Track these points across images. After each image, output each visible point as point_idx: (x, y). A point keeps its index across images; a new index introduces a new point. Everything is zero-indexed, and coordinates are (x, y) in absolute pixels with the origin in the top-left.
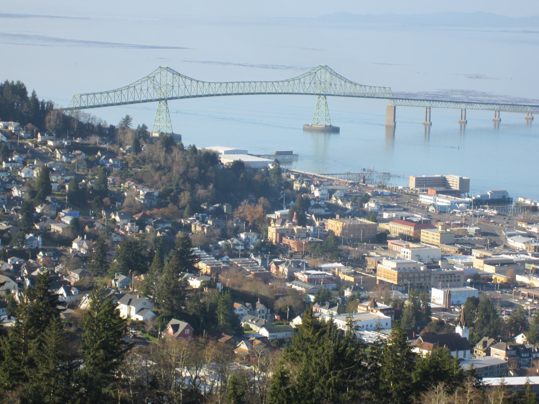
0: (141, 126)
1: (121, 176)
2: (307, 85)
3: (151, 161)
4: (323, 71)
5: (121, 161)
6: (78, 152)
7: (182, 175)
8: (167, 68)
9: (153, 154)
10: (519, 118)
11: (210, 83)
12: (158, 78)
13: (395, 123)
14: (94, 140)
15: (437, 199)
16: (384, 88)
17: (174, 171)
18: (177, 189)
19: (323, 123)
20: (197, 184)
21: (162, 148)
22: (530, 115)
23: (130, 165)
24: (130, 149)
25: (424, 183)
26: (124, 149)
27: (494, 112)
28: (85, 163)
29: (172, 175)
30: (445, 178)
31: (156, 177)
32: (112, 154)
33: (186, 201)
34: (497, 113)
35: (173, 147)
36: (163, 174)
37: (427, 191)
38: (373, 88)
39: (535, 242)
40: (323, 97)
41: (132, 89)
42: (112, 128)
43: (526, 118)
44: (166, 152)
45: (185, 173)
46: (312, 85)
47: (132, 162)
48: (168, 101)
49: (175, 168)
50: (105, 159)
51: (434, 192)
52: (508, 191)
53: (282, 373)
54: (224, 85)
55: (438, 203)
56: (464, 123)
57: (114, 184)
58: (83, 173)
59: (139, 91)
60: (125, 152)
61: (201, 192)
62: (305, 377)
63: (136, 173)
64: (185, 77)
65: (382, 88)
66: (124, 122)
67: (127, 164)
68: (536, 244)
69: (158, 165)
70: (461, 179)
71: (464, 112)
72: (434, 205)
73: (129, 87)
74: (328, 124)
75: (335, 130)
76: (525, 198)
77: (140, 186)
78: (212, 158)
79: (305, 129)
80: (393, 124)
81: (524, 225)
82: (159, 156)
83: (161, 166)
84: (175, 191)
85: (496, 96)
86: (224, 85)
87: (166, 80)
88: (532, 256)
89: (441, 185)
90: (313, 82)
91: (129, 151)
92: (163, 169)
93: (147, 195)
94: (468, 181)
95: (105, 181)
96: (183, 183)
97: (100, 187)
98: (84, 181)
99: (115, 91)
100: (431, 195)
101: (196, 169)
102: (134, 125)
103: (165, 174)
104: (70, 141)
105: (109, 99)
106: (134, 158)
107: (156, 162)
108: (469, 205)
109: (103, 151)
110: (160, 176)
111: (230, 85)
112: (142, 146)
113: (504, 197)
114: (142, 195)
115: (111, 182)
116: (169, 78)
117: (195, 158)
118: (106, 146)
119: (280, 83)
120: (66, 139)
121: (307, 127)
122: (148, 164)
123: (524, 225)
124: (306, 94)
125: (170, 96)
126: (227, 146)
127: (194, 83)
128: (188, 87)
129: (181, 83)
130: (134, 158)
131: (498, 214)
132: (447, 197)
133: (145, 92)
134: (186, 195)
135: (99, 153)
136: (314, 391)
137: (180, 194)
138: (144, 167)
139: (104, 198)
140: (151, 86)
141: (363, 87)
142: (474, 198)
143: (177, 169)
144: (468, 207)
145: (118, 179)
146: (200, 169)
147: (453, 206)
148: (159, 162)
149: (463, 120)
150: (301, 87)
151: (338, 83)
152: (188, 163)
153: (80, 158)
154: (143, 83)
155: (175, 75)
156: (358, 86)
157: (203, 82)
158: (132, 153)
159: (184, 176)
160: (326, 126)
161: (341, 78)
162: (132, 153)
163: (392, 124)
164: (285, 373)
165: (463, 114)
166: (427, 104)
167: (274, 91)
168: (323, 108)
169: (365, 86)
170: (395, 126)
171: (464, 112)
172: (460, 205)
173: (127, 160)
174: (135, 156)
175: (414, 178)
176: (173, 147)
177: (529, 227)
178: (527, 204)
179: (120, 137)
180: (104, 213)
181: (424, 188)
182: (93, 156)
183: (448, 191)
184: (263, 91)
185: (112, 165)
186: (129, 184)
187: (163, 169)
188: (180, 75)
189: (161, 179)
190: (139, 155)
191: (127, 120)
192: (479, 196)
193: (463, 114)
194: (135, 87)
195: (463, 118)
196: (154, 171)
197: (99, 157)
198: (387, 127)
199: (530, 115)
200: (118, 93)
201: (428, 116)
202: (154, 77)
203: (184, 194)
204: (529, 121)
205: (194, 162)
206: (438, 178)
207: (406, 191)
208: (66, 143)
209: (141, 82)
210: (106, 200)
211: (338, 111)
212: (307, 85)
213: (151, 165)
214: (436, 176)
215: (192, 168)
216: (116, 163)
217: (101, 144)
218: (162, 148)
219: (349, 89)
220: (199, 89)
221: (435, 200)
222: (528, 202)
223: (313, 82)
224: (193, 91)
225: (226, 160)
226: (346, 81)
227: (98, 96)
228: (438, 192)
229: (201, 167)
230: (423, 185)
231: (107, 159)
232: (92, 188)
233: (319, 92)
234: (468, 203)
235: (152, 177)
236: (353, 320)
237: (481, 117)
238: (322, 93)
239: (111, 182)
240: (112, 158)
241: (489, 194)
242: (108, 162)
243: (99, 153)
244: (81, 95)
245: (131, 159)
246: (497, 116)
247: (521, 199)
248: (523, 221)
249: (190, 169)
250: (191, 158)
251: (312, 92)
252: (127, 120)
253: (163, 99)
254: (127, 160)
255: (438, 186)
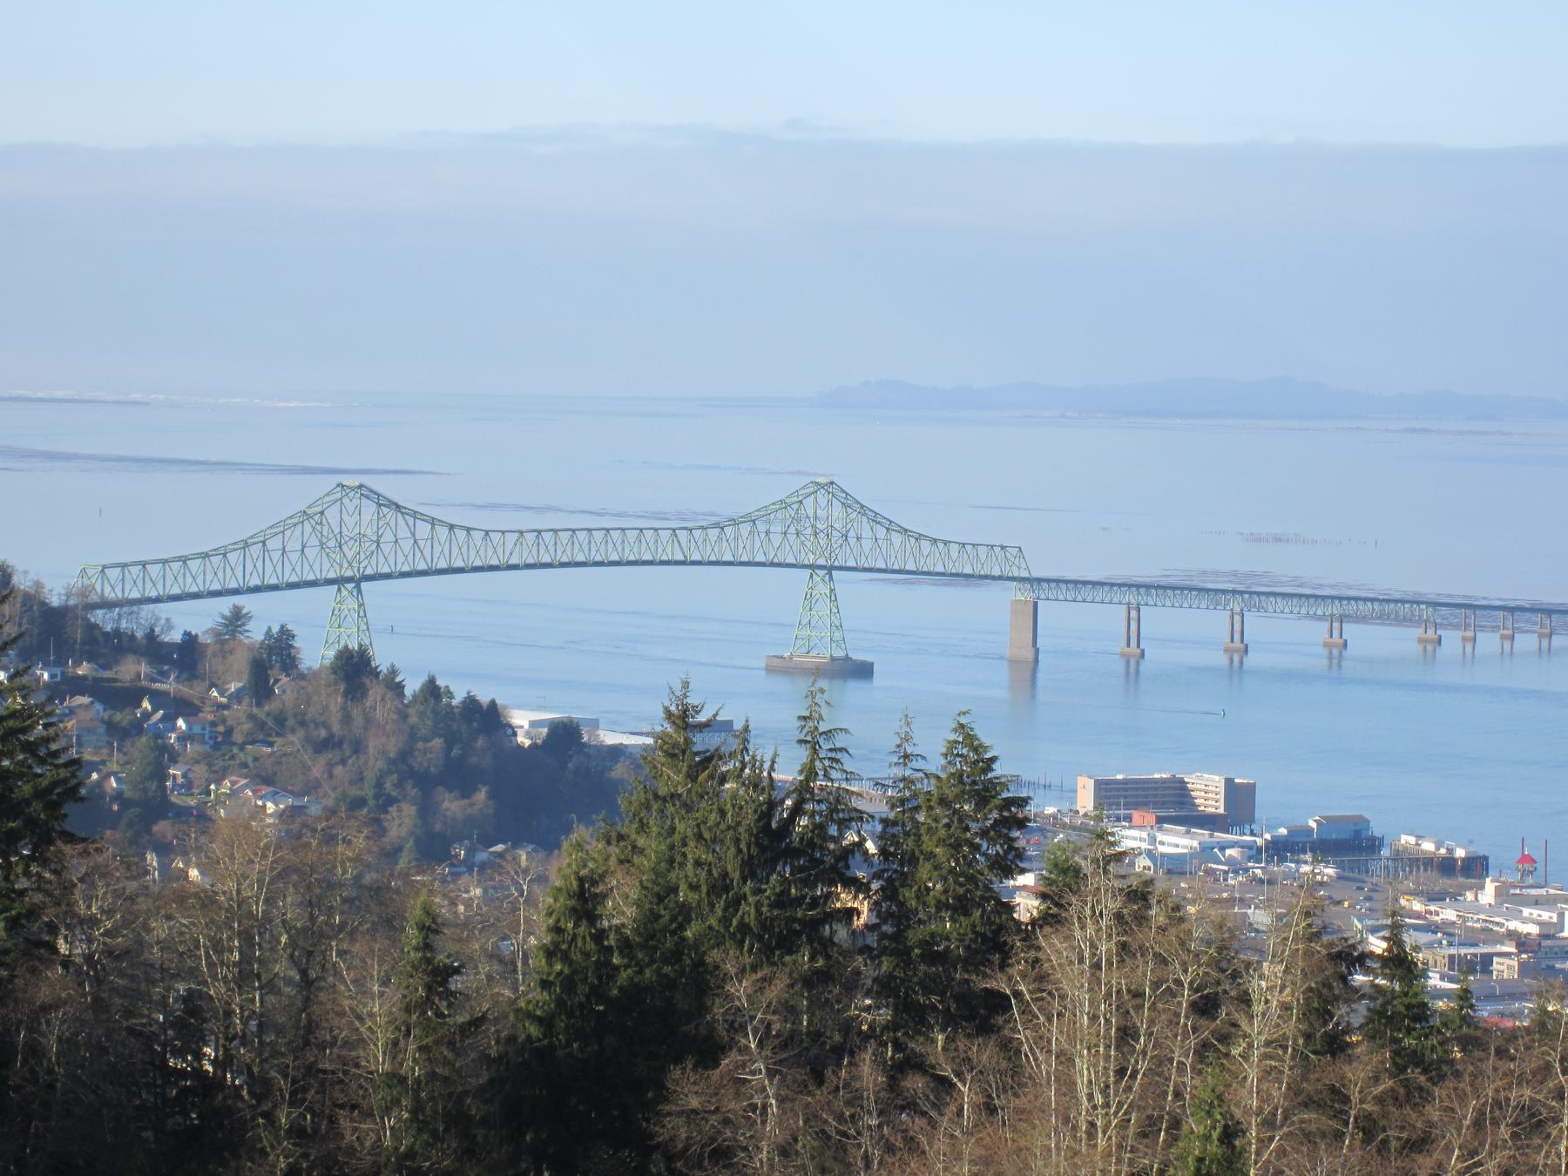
0: (275, 629)
1: (210, 765)
2: (777, 540)
3: (303, 724)
4: (822, 498)
5: (213, 724)
6: (85, 700)
7: (394, 762)
8: (361, 486)
9: (308, 705)
10: (1401, 641)
11: (487, 532)
12: (332, 515)
13: (1037, 651)
14: (131, 669)
15: (1160, 837)
16: (1003, 547)
17: (371, 751)
18: (377, 797)
19: (824, 652)
20: (440, 789)
21: (336, 684)
22: (1431, 632)
23: (238, 737)
24: (239, 691)
25: (1119, 797)
26: (222, 694)
27: (1326, 625)
28: (102, 729)
29: (366, 762)
30: (1182, 782)
31: (317, 771)
32: (185, 707)
33: (404, 831)
34: (1336, 625)
35: (366, 681)
36: (338, 759)
37: (1129, 818)
38: (969, 548)
39: (1450, 944)
40: (822, 573)
41: (256, 550)
42: (190, 641)
43: (1421, 641)
44: (346, 694)
45: (404, 756)
46: (792, 538)
47: (247, 726)
48: (364, 585)
49: (373, 744)
50: (162, 720)
51: (1150, 818)
52: (1367, 816)
53: (581, 880)
54: (530, 537)
55: (1162, 849)
56: (1240, 649)
57: (188, 785)
58: (96, 759)
59: (276, 555)
60: (224, 700)
61: (451, 806)
62: (657, 889)
63: (256, 759)
64: (415, 515)
65: (997, 550)
66: (226, 626)
67: (229, 732)
68: (1453, 951)
69: (323, 733)
70: (1229, 783)
71: (1237, 618)
72: (1150, 854)
73: (246, 545)
74: (841, 654)
75: (863, 671)
76: (1419, 837)
77: (265, 790)
78: (488, 718)
79: (770, 670)
80: (1030, 655)
81: (1417, 906)
82: (326, 708)
83: (332, 735)
84: (372, 803)
85: (1332, 586)
86: (530, 537)
87: (359, 523)
88: (1442, 979)
89: (1172, 803)
90: (792, 530)
91: (237, 697)
92: (339, 744)
93: (287, 816)
94: (1251, 788)
95: (162, 776)
96: (399, 785)
97: (145, 790)
98: (95, 776)
99: (205, 556)
100: (1141, 827)
101: (438, 743)
102: (256, 632)
103: (343, 762)
104: (58, 671)
105: (189, 580)
106: (251, 717)
107: (317, 725)
108: (1253, 852)
109: (158, 698)
110: (330, 766)
111: (547, 536)
112: (277, 681)
113: (1358, 833)
114: (271, 815)
115: (180, 780)
116: (366, 518)
117: (435, 712)
118: (170, 685)
119: (697, 533)
120: (46, 666)
121: (777, 662)
122: (293, 731)
123: (1417, 906)
124: (772, 564)
125: (369, 571)
126: (539, 708)
127: (443, 532)
128: (422, 544)
129: (403, 532)
130: (251, 717)
131: (1340, 878)
132: (1188, 832)
133: (295, 557)
134: (405, 813)
135: (146, 704)
136: (689, 934)
137: (387, 812)
138: (279, 741)
139: (155, 822)
140: (314, 541)
141: (941, 545)
142: (1268, 836)
143: (381, 746)
144: (1250, 859)
145: (200, 771)
146: (450, 743)
147: (1206, 851)
148: (325, 725)
149: (1237, 644)
150: (758, 544)
151: (867, 533)
152: (412, 728)
153: (85, 716)
154: (288, 533)
155: (385, 510)
156: (925, 545)
157: (468, 530)
158: (246, 701)
159: (402, 763)
160: (833, 659)
161: (875, 518)
162: (246, 701)
163: (1028, 654)
164: (594, 883)
165: (1237, 627)
166: (1130, 597)
167: (680, 557)
168: (823, 608)
169: (946, 543)
170: (1036, 661)
171: (1237, 618)
172: (1228, 852)
173: (230, 722)
174: (255, 710)
175: (1092, 782)
176: (366, 681)
177: (1432, 908)
178: (1425, 852)
179: (208, 664)
180: (152, 859)
181: (1122, 812)
182: (128, 710)
183: (1193, 819)
184: (648, 557)
185: (183, 738)
186: (233, 783)
187: (339, 744)
188: (398, 506)
189: (331, 776)
190: (266, 708)
191: (237, 619)
192: (1283, 831)
193: (1237, 627)
194: (264, 543)
195: (1237, 637)
196: (310, 750)
197: (147, 716)
198: (1014, 662)
199: (1431, 632)
200: (216, 560)
201: (1134, 635)
202: (322, 513)
203: (400, 810)
204: (1430, 647)
205: (430, 723)
206: (1163, 781)
207: (1067, 820)
208: (46, 676)
209: (281, 528)
210: (163, 828)
211: (870, 614)
212: (777, 540)
213: (301, 733)
214: (1156, 776)
215: (427, 740)
216: (197, 729)
217: (153, 680)
218: (336, 684)
219: (899, 552)
220: (455, 550)
221: (1153, 840)
222: (1428, 846)
223: (792, 530)
224: (436, 555)
225: (525, 722)
226: (891, 526)
227: (154, 570)
228: (1161, 820)
229: (451, 739)
230: (1118, 804)
231: (170, 719)
232: (118, 796)
233: (810, 559)
234: (1250, 848)
235: (306, 769)
236: (823, 727)
237: (1286, 638)
238: (822, 562)
239: (180, 780)
240: (185, 716)
241: (1313, 825)
242: (174, 728)
243: (146, 704)
244: (104, 567)
245: (243, 719)
246: (1336, 633)
247: (1407, 840)
248: (1414, 893)
249: (420, 745)
250: (422, 715)
251: (791, 560)
252: (237, 619)
253: (350, 580)
254: (230, 722)
255: (1163, 805)
